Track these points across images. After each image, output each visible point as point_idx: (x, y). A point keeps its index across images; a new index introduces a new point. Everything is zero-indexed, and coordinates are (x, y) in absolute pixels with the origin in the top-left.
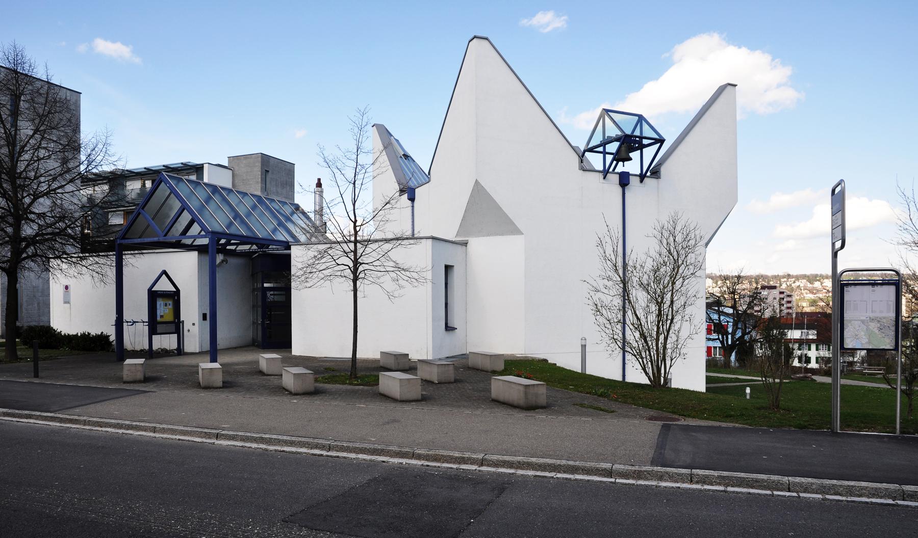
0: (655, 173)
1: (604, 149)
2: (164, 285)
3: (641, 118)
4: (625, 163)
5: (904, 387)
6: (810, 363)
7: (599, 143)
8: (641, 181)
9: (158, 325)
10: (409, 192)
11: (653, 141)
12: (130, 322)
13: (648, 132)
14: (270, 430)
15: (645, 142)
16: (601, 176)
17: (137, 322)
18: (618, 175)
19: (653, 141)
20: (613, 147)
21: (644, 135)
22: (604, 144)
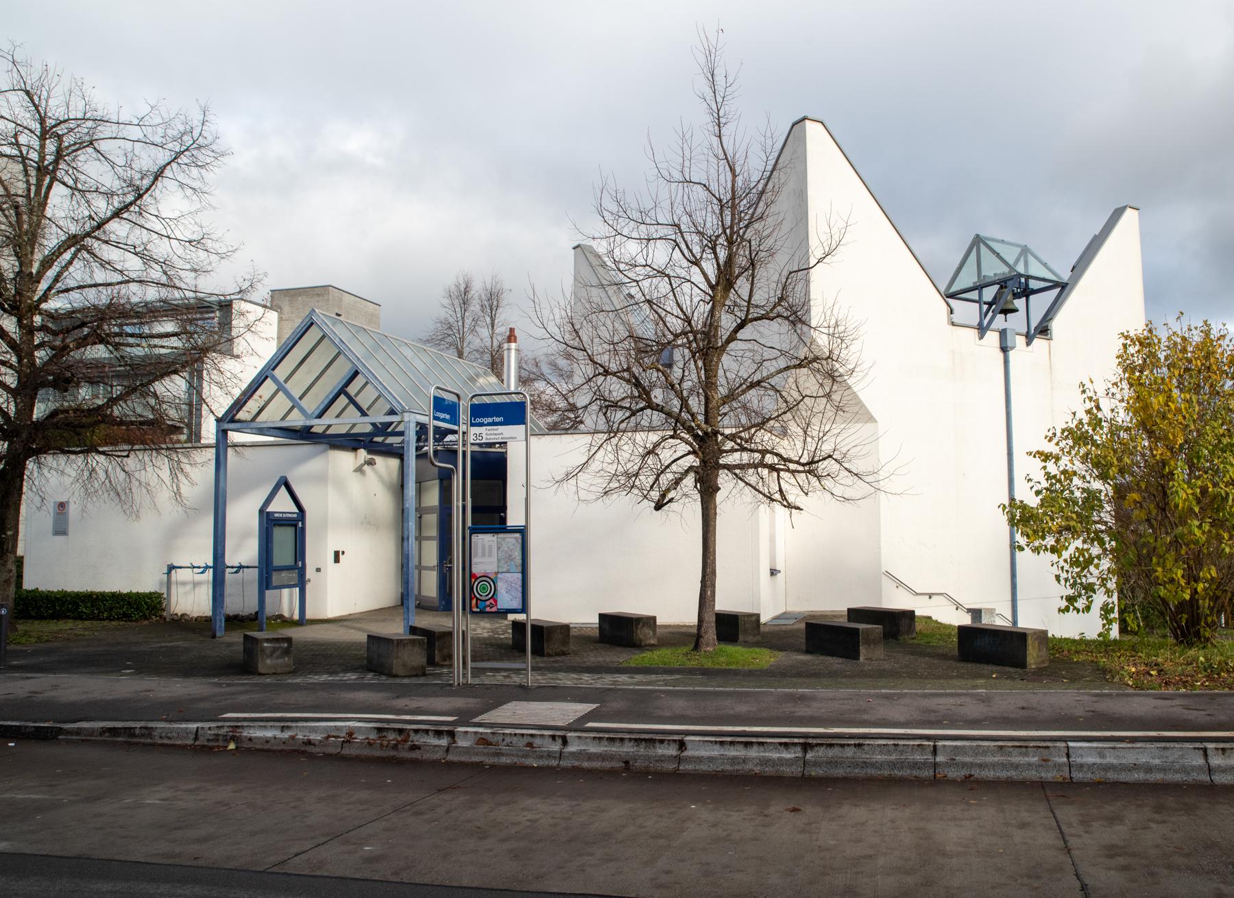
0: (1043, 330)
1: (980, 295)
2: (282, 505)
3: (1025, 251)
4: (1008, 315)
5: (360, 737)
6: (654, 618)
7: (972, 285)
8: (1028, 344)
9: (422, 594)
10: (510, 304)
11: (975, 249)
12: (199, 567)
13: (1036, 270)
14: (1151, 769)
15: (1033, 284)
16: (974, 333)
17: (180, 567)
18: (998, 333)
19: (975, 249)
20: (989, 293)
21: (1032, 272)
22: (979, 287)
